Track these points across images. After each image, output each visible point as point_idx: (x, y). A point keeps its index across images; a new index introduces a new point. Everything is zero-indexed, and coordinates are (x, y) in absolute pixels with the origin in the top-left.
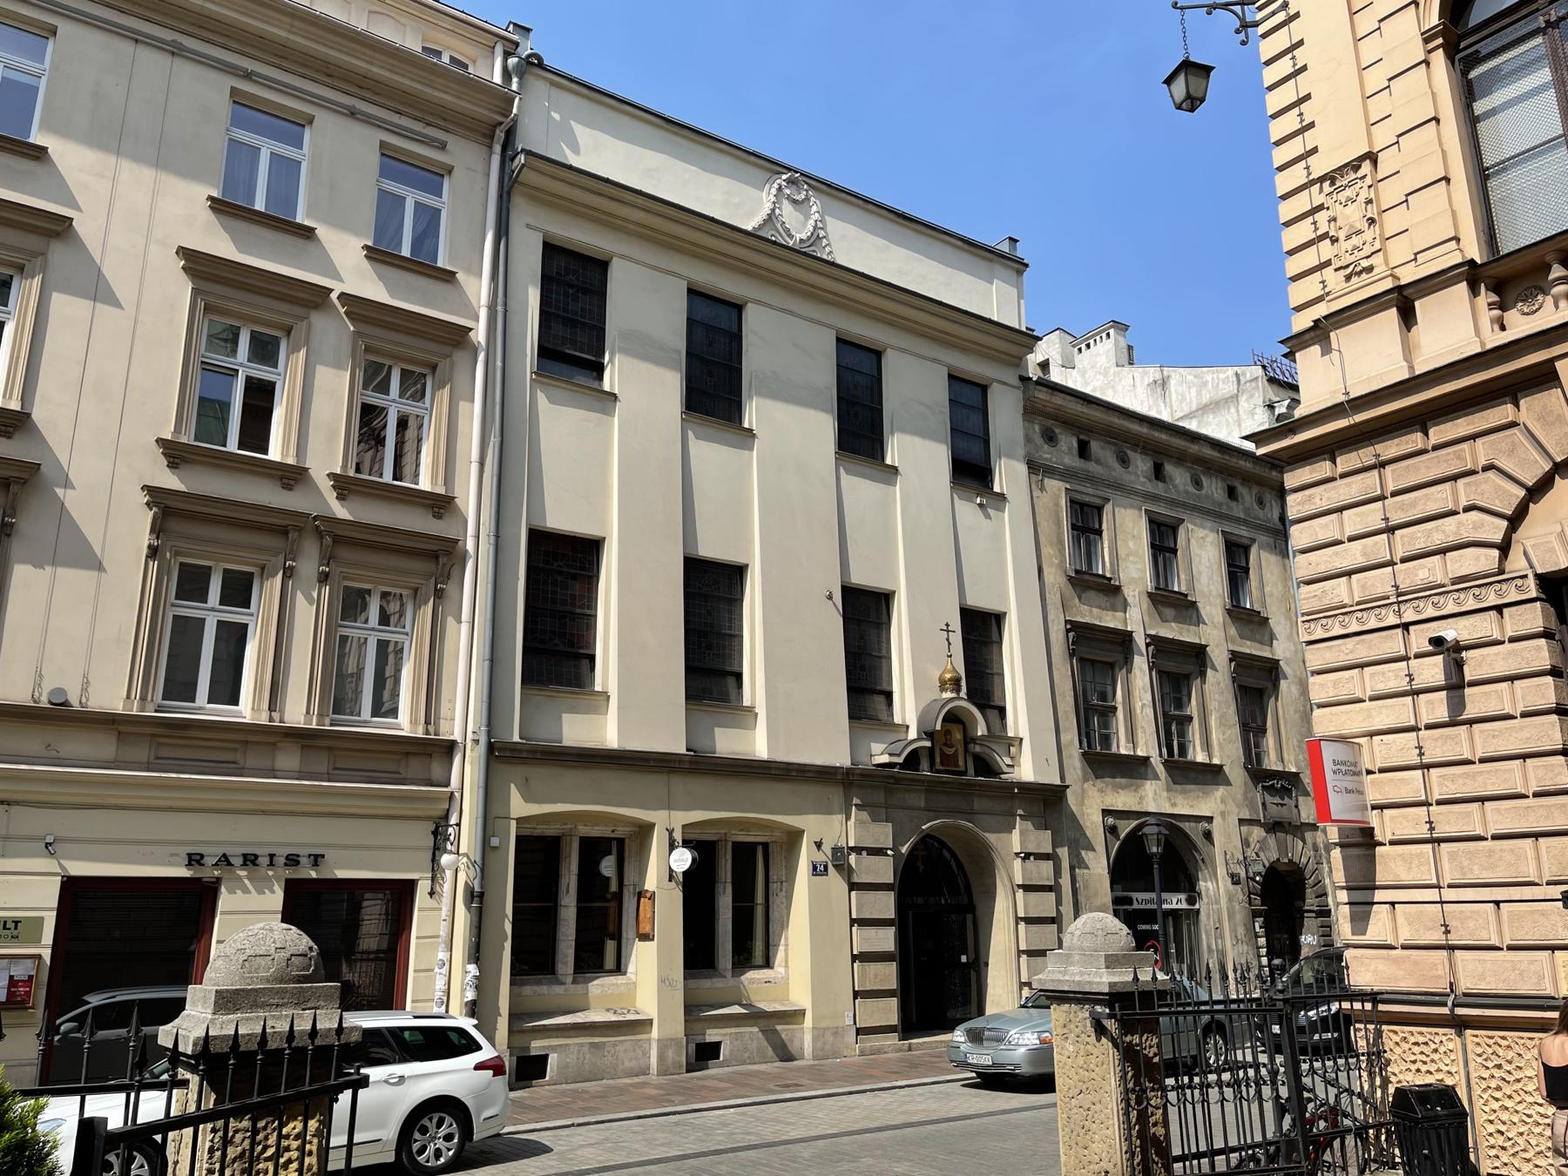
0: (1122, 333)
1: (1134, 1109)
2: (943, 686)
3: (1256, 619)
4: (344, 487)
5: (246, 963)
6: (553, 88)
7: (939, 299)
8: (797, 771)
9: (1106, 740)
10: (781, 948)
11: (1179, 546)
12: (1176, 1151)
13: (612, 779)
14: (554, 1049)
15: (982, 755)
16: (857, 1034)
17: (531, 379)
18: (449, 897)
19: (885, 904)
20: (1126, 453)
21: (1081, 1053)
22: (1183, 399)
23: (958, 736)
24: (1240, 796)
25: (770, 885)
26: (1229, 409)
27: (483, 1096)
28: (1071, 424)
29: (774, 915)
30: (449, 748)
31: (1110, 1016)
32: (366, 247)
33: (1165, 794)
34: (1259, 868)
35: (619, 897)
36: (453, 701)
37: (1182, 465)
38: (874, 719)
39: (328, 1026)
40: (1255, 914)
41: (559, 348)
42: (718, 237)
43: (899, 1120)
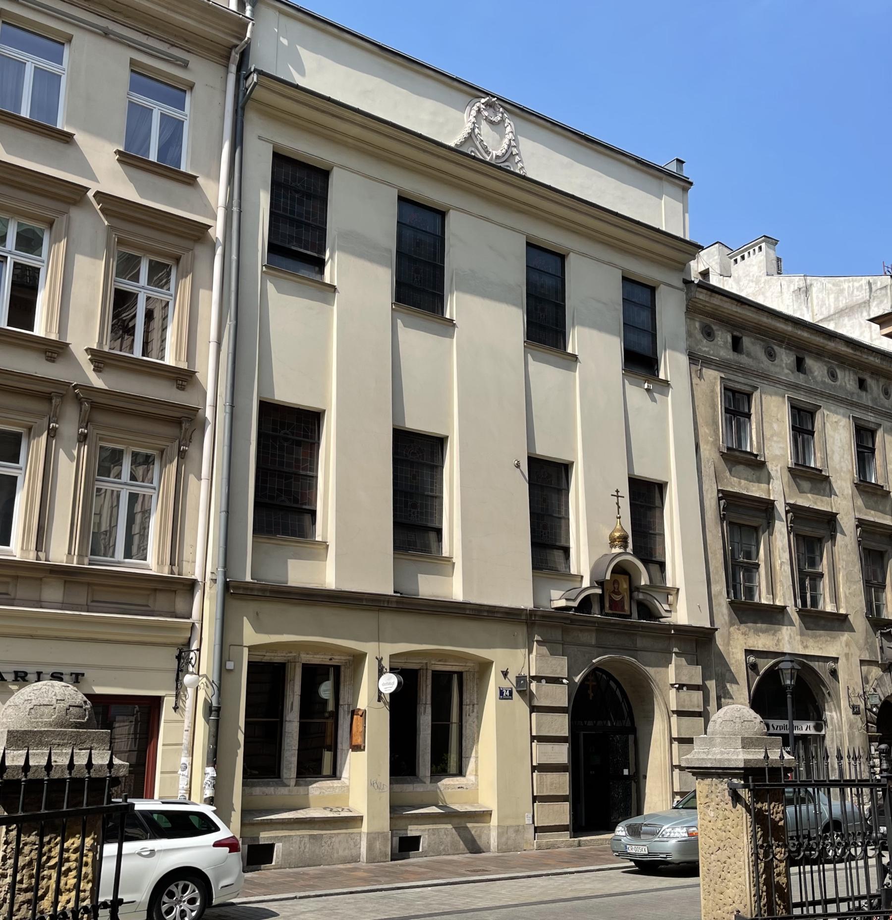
0: (772, 246)
1: (762, 860)
2: (612, 542)
3: (879, 492)
4: (99, 360)
5: (32, 711)
6: (281, 15)
7: (616, 210)
8: (488, 611)
9: (750, 592)
10: (472, 760)
11: (816, 429)
12: (796, 899)
13: (328, 614)
14: (279, 839)
15: (646, 602)
16: (535, 832)
17: (262, 272)
18: (191, 712)
19: (560, 725)
20: (773, 349)
21: (721, 817)
22: (823, 304)
23: (625, 586)
24: (862, 641)
25: (464, 707)
26: (862, 313)
27: (222, 869)
28: (727, 322)
29: (466, 732)
30: (191, 586)
31: (745, 786)
32: (118, 152)
33: (798, 638)
34: (876, 701)
35: (335, 715)
36: (194, 546)
37: (821, 360)
38: (554, 569)
39: (100, 762)
40: (871, 739)
41: (287, 246)
42: (424, 151)
43: (570, 895)
